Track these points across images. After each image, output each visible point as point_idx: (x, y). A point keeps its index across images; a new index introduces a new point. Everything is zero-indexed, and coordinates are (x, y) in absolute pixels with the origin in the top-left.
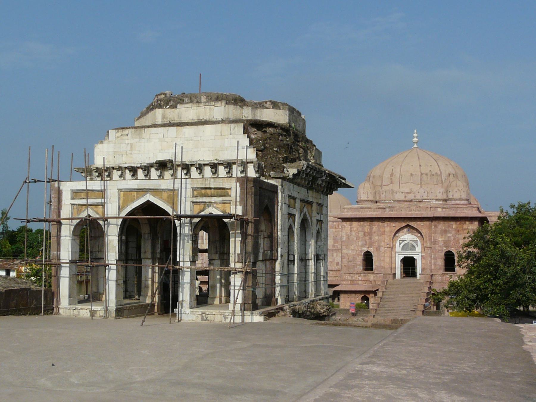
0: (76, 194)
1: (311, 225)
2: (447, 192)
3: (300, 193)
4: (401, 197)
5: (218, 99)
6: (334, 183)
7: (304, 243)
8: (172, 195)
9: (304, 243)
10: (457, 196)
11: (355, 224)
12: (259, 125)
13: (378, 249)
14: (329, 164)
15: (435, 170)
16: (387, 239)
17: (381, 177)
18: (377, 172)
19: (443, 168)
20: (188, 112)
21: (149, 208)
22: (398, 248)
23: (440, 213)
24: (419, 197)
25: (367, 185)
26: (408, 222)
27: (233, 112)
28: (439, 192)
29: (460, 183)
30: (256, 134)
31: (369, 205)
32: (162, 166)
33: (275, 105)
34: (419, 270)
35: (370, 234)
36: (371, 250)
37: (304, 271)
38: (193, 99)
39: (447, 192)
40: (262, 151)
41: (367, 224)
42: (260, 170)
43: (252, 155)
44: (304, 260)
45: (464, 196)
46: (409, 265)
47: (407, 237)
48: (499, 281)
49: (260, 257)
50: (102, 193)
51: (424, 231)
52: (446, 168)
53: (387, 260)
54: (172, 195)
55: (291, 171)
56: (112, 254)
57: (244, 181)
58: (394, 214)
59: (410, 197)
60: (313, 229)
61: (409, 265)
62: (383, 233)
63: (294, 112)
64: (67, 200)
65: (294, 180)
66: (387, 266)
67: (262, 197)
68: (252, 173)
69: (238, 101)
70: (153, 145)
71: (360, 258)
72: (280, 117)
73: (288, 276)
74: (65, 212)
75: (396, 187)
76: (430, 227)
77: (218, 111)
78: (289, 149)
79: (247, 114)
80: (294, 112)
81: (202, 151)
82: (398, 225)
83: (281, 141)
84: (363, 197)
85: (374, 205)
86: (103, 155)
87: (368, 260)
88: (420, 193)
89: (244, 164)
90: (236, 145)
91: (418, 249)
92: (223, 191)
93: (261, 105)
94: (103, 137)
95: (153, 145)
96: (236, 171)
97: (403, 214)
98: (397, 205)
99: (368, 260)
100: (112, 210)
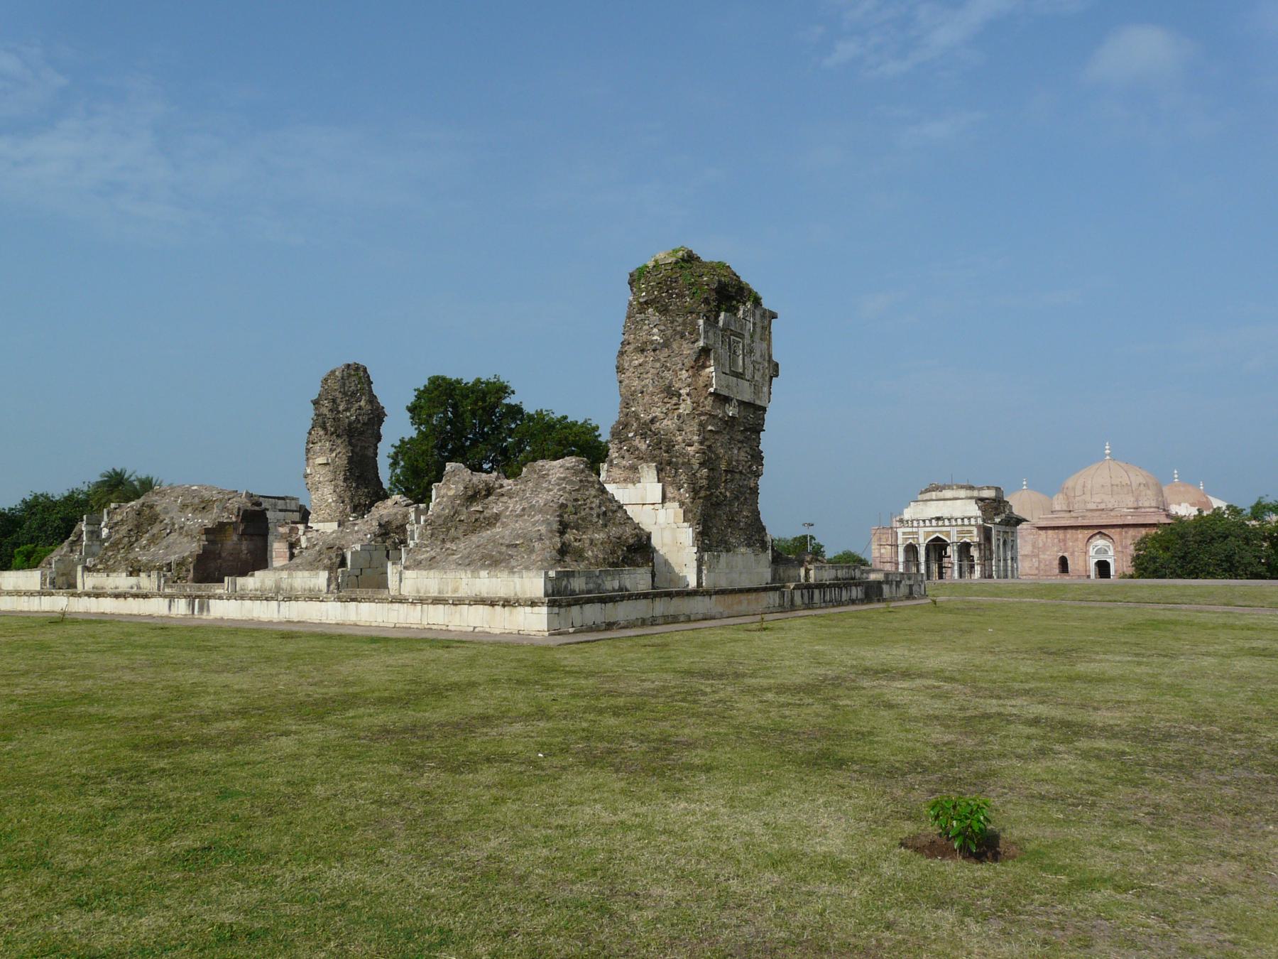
0: (904, 533)
1: (1009, 543)
2: (1137, 500)
3: (1002, 528)
4: (1093, 506)
5: (962, 487)
6: (1019, 521)
7: (1005, 552)
8: (948, 534)
9: (1005, 552)
10: (1147, 504)
11: (1050, 532)
12: (982, 500)
13: (1072, 554)
14: (1017, 511)
15: (1126, 480)
16: (1081, 545)
17: (1074, 489)
18: (1070, 483)
19: (1133, 479)
20: (948, 493)
21: (938, 539)
22: (1092, 552)
23: (1130, 520)
24: (1110, 506)
25: (1061, 496)
26: (1100, 530)
27: (969, 493)
28: (1130, 501)
29: (1150, 493)
30: (981, 504)
31: (1063, 515)
32: (938, 519)
33: (988, 488)
34: (1112, 572)
35: (1064, 540)
36: (1066, 555)
37: (1006, 565)
38: (950, 487)
39: (1137, 500)
40: (984, 511)
41: (1061, 532)
42: (984, 521)
43: (979, 513)
44: (1005, 560)
45: (1154, 504)
46: (1103, 568)
47: (1100, 542)
48: (451, 493)
49: (986, 558)
50: (917, 533)
51: (1116, 537)
52: (1137, 477)
53: (1081, 563)
54: (948, 534)
55: (997, 520)
56: (922, 558)
57: (979, 527)
58: (1086, 523)
59: (1102, 506)
60: (1010, 544)
61: (1103, 568)
62: (1077, 540)
63: (998, 489)
64: (900, 535)
65: (999, 524)
66: (1082, 569)
67: (986, 533)
68: (980, 522)
69: (971, 488)
70: (933, 510)
71: (1057, 562)
72: (989, 494)
73: (998, 566)
74: (900, 541)
75: (1087, 497)
76: (1120, 533)
77: (963, 493)
78: (996, 509)
79: (975, 494)
80: (998, 489)
81: (958, 512)
82: (1091, 532)
83: (994, 506)
84: (1057, 508)
85: (1068, 515)
86: (908, 514)
87: (1064, 564)
88: (1111, 502)
89: (976, 518)
90: (973, 510)
91: (1111, 553)
92: (970, 532)
93: (982, 489)
94: (908, 505)
95: (933, 510)
96: (973, 521)
97: (1095, 522)
98: (1089, 514)
99: (1064, 564)
100: (921, 540)
